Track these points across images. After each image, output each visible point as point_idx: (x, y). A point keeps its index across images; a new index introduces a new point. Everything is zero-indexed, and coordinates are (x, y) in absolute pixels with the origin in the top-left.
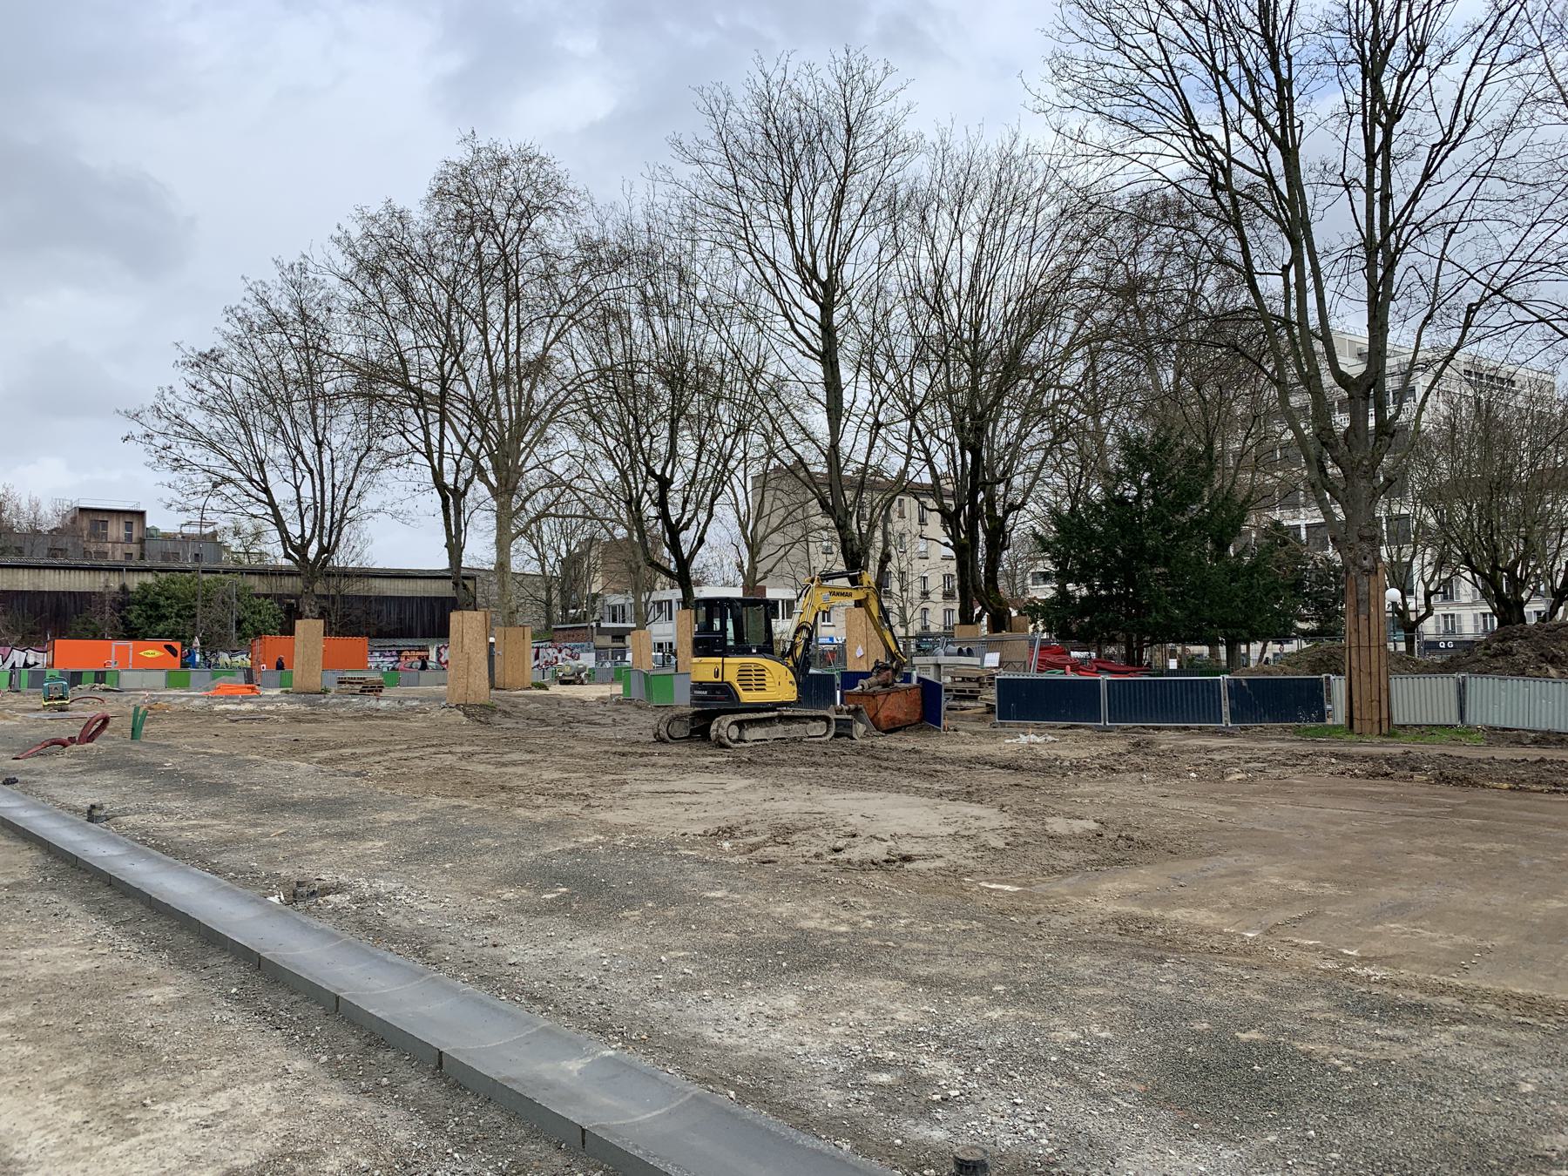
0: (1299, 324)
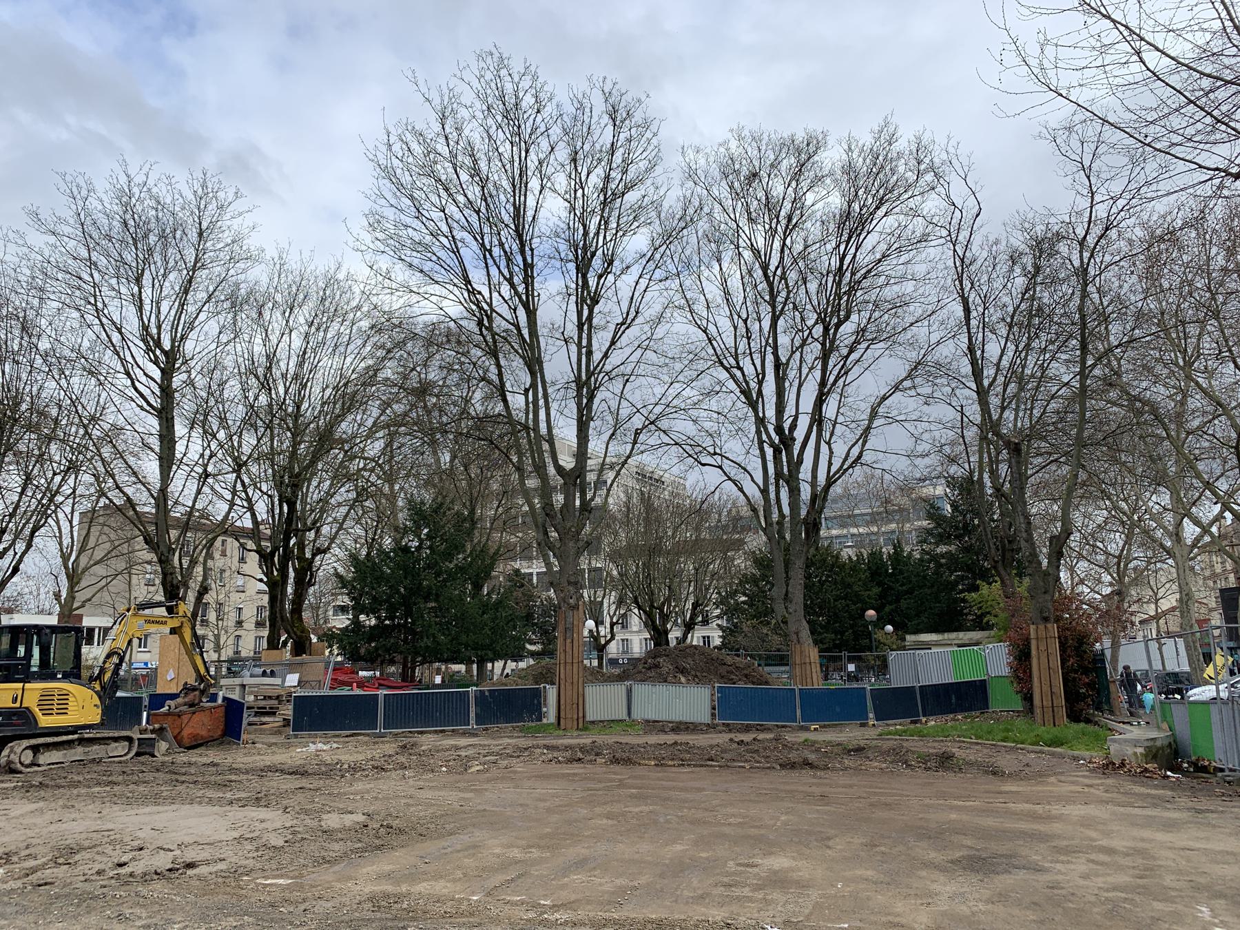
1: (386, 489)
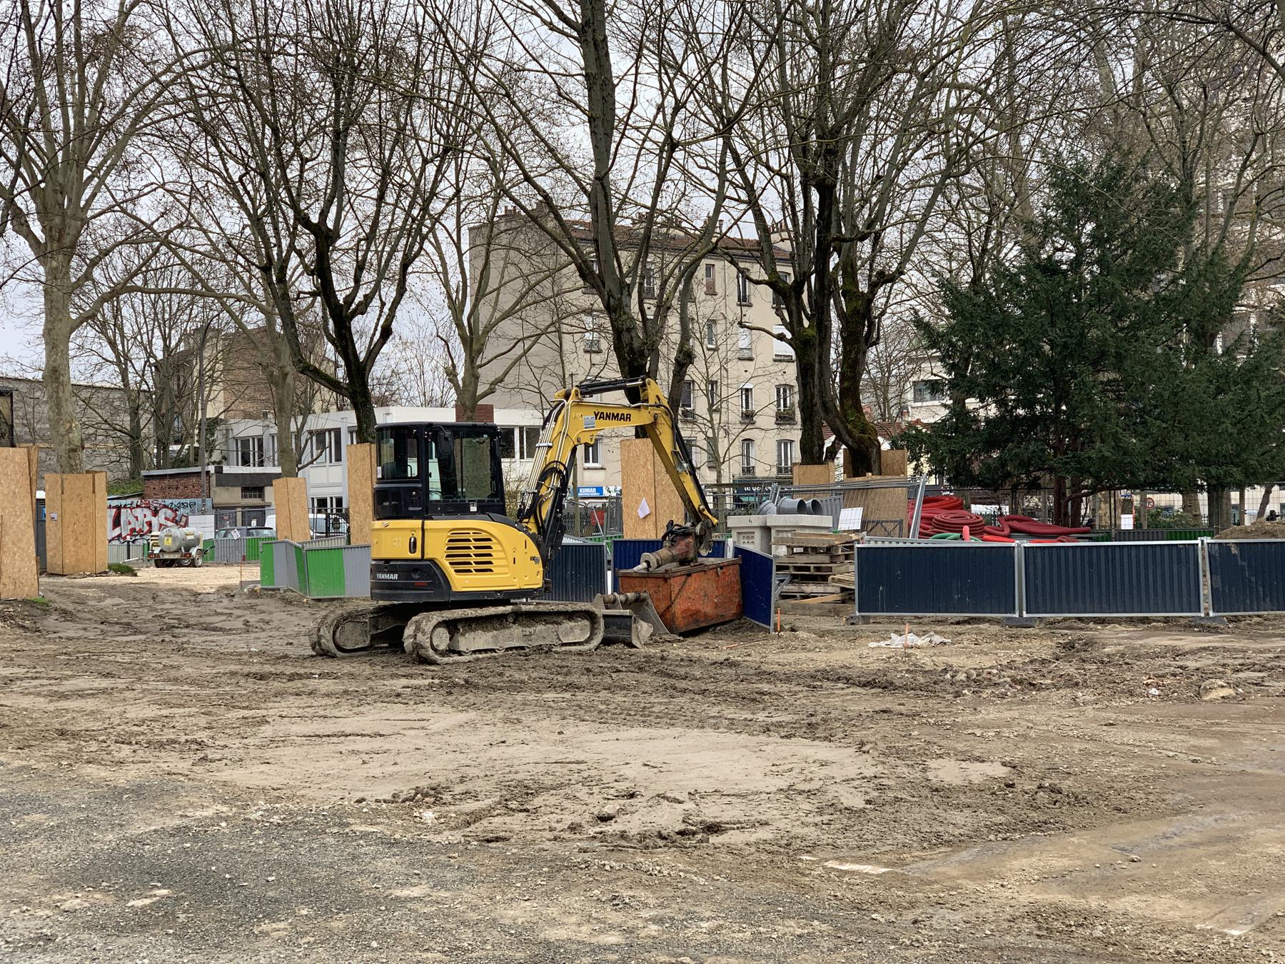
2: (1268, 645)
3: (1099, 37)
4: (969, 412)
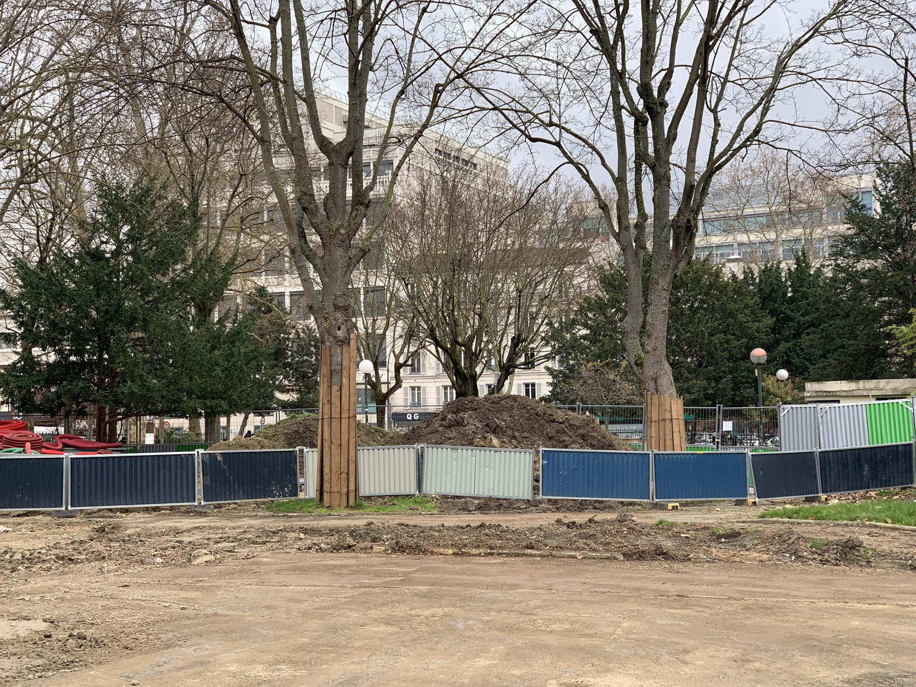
0: (284, 82)
1: (65, 164)
2: (239, 524)
3: (133, 96)
4: (33, 357)
